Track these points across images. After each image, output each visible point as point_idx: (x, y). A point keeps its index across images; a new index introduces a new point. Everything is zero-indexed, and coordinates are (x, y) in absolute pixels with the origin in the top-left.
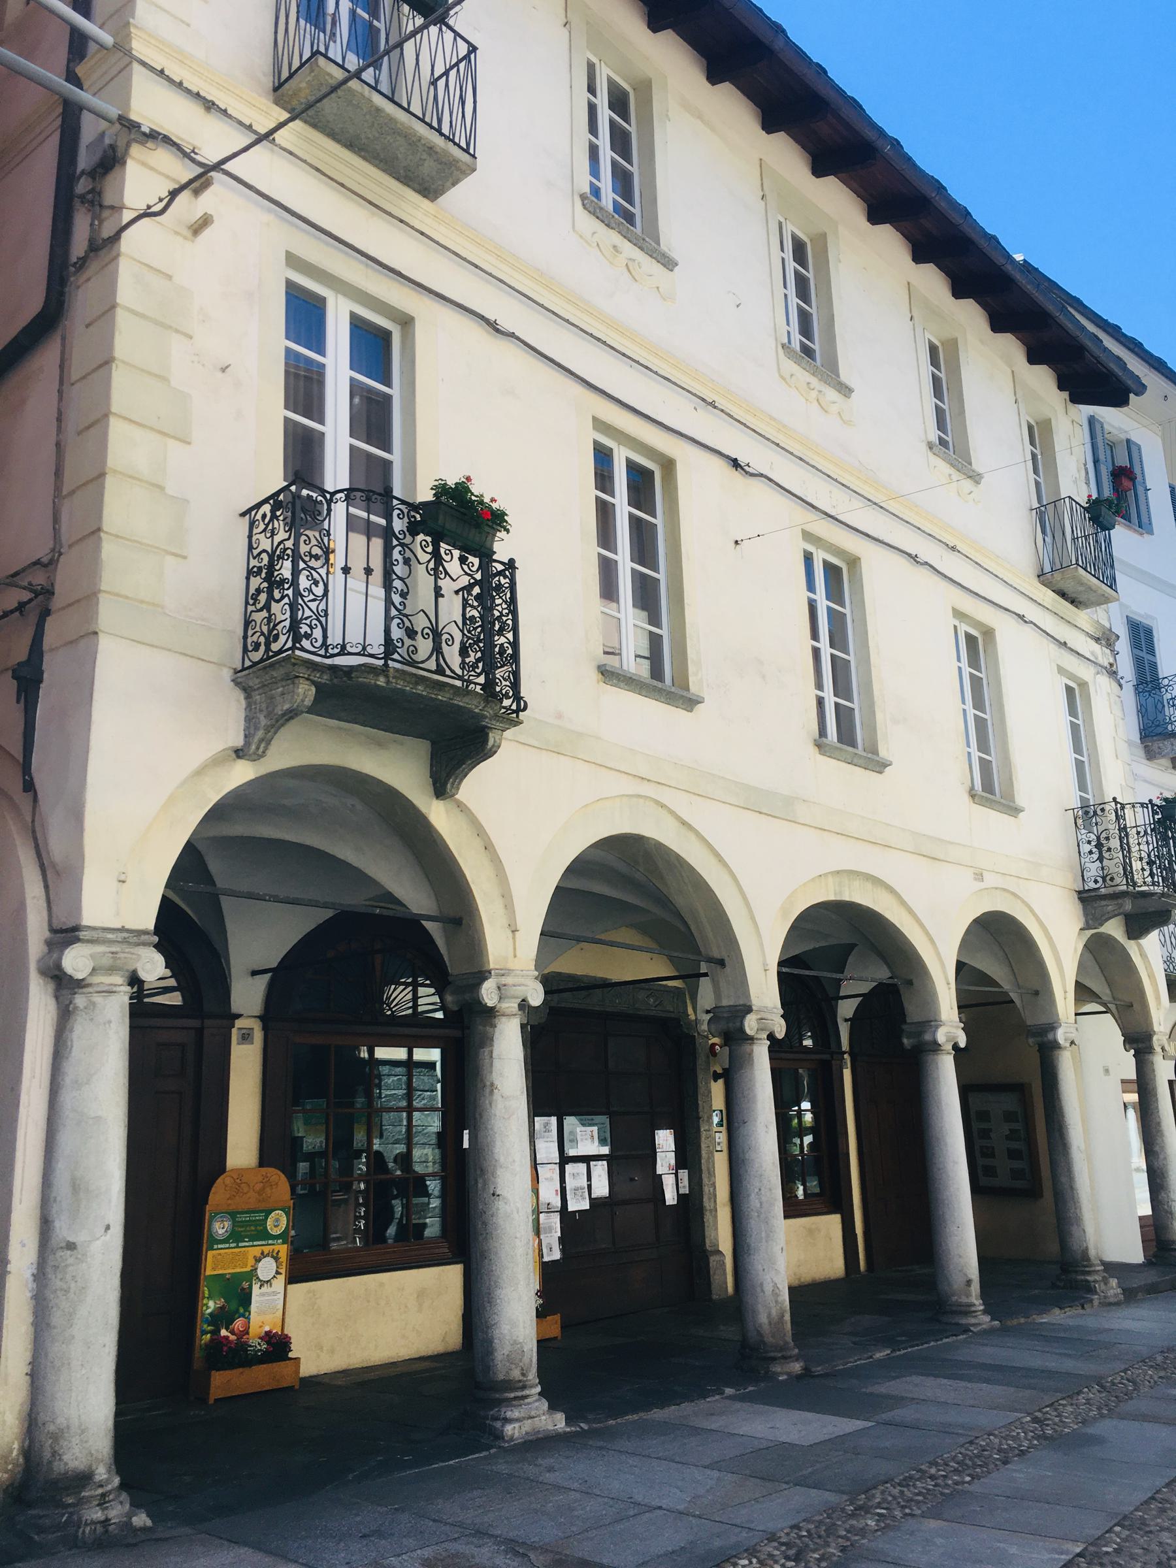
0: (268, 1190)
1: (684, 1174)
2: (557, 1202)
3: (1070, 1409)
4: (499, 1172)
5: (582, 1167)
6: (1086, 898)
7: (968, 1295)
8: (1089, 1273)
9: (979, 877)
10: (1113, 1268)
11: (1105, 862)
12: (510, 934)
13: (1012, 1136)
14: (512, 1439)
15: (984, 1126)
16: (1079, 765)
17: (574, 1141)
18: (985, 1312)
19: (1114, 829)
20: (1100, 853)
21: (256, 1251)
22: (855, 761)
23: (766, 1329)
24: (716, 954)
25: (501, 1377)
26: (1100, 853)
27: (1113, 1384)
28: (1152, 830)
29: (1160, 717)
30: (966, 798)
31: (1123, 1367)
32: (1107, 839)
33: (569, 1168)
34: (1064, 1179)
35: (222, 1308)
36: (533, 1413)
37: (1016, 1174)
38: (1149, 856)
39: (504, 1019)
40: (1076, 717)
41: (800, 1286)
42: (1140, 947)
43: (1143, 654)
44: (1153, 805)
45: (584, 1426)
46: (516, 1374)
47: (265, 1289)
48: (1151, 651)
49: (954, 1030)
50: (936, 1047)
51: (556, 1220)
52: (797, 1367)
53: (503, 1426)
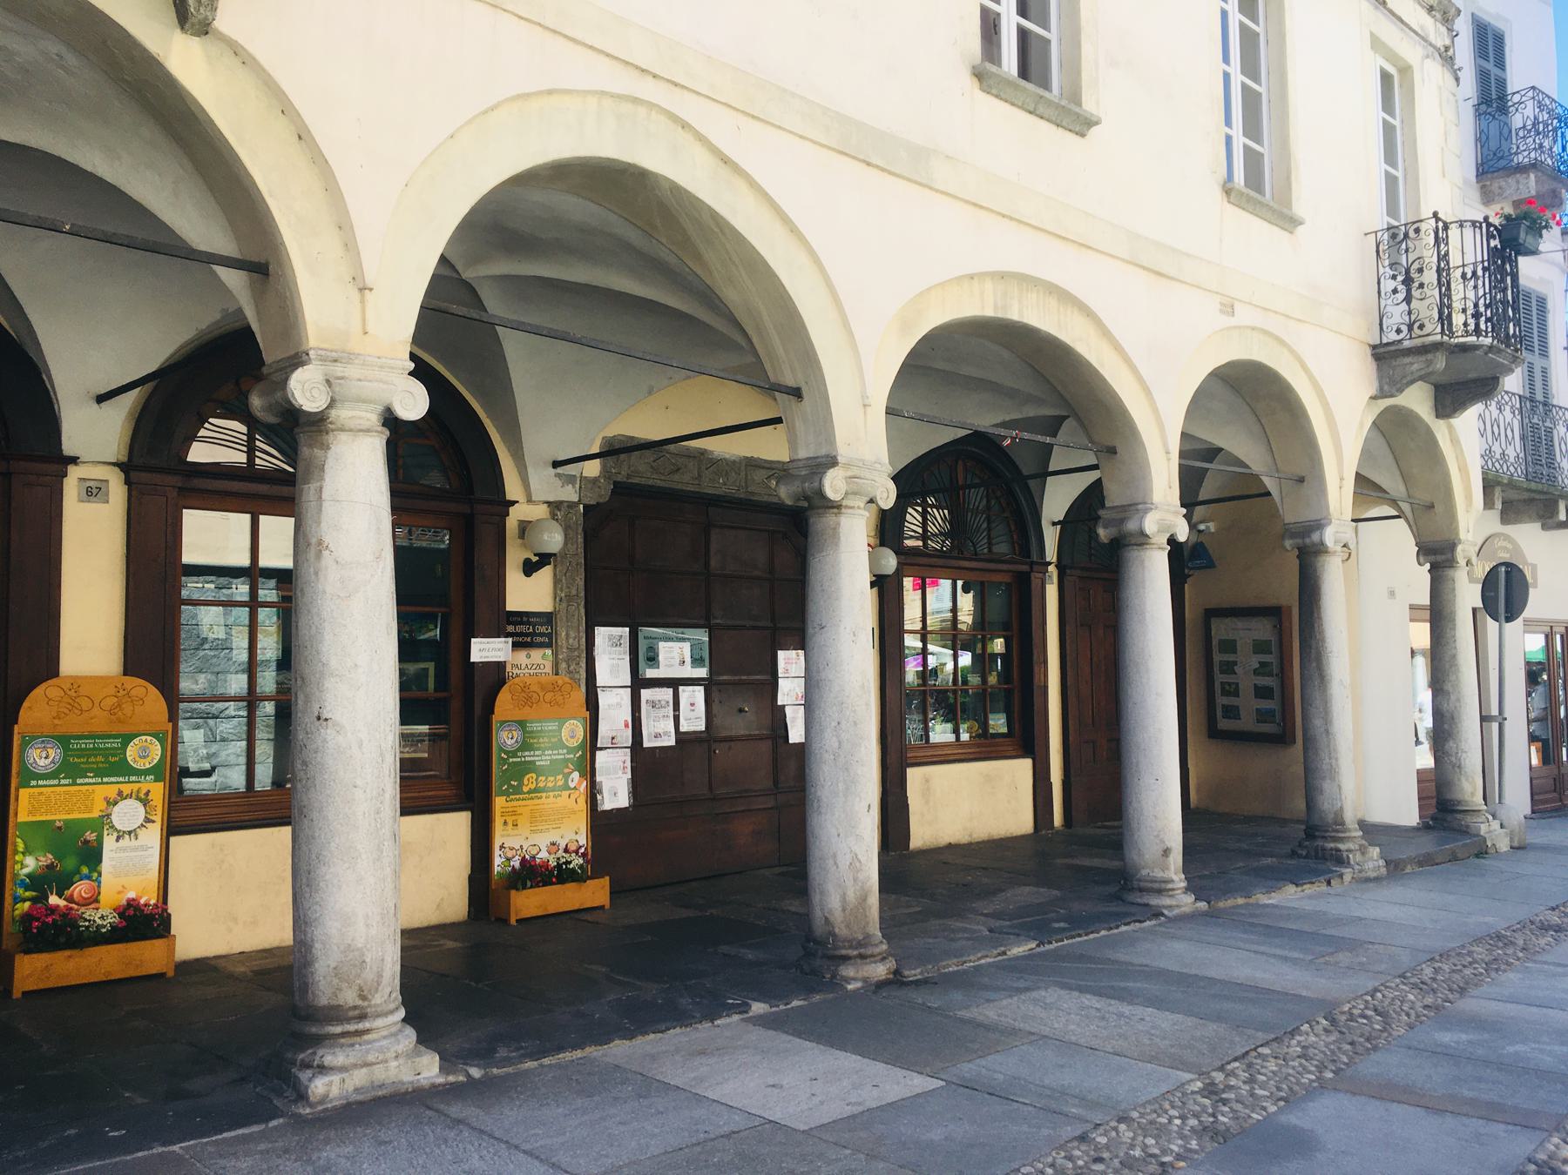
0: (127, 708)
2: (626, 737)
3: (1272, 1065)
5: (667, 694)
6: (1383, 355)
7: (1165, 868)
8: (1341, 840)
9: (1229, 309)
10: (1372, 831)
11: (1414, 304)
12: (356, 295)
13: (1263, 669)
14: (322, 1101)
15: (1230, 658)
16: (1391, 181)
17: (653, 660)
18: (1187, 890)
19: (1431, 258)
20: (1409, 291)
21: (111, 791)
22: (1041, 110)
23: (838, 916)
24: (790, 381)
25: (323, 1001)
26: (1409, 291)
27: (1352, 1018)
28: (1484, 269)
29: (1505, 145)
30: (1218, 194)
31: (1370, 985)
32: (1420, 270)
33: (646, 694)
34: (1318, 722)
35: (51, 867)
36: (371, 1058)
37: (1263, 716)
38: (1476, 305)
39: (343, 437)
40: (1392, 114)
41: (970, 844)
42: (1451, 428)
43: (1490, 66)
44: (1489, 225)
45: (476, 1073)
46: (349, 997)
47: (125, 842)
48: (1500, 63)
49: (1170, 518)
50: (1142, 539)
51: (625, 756)
52: (880, 971)
53: (310, 1080)
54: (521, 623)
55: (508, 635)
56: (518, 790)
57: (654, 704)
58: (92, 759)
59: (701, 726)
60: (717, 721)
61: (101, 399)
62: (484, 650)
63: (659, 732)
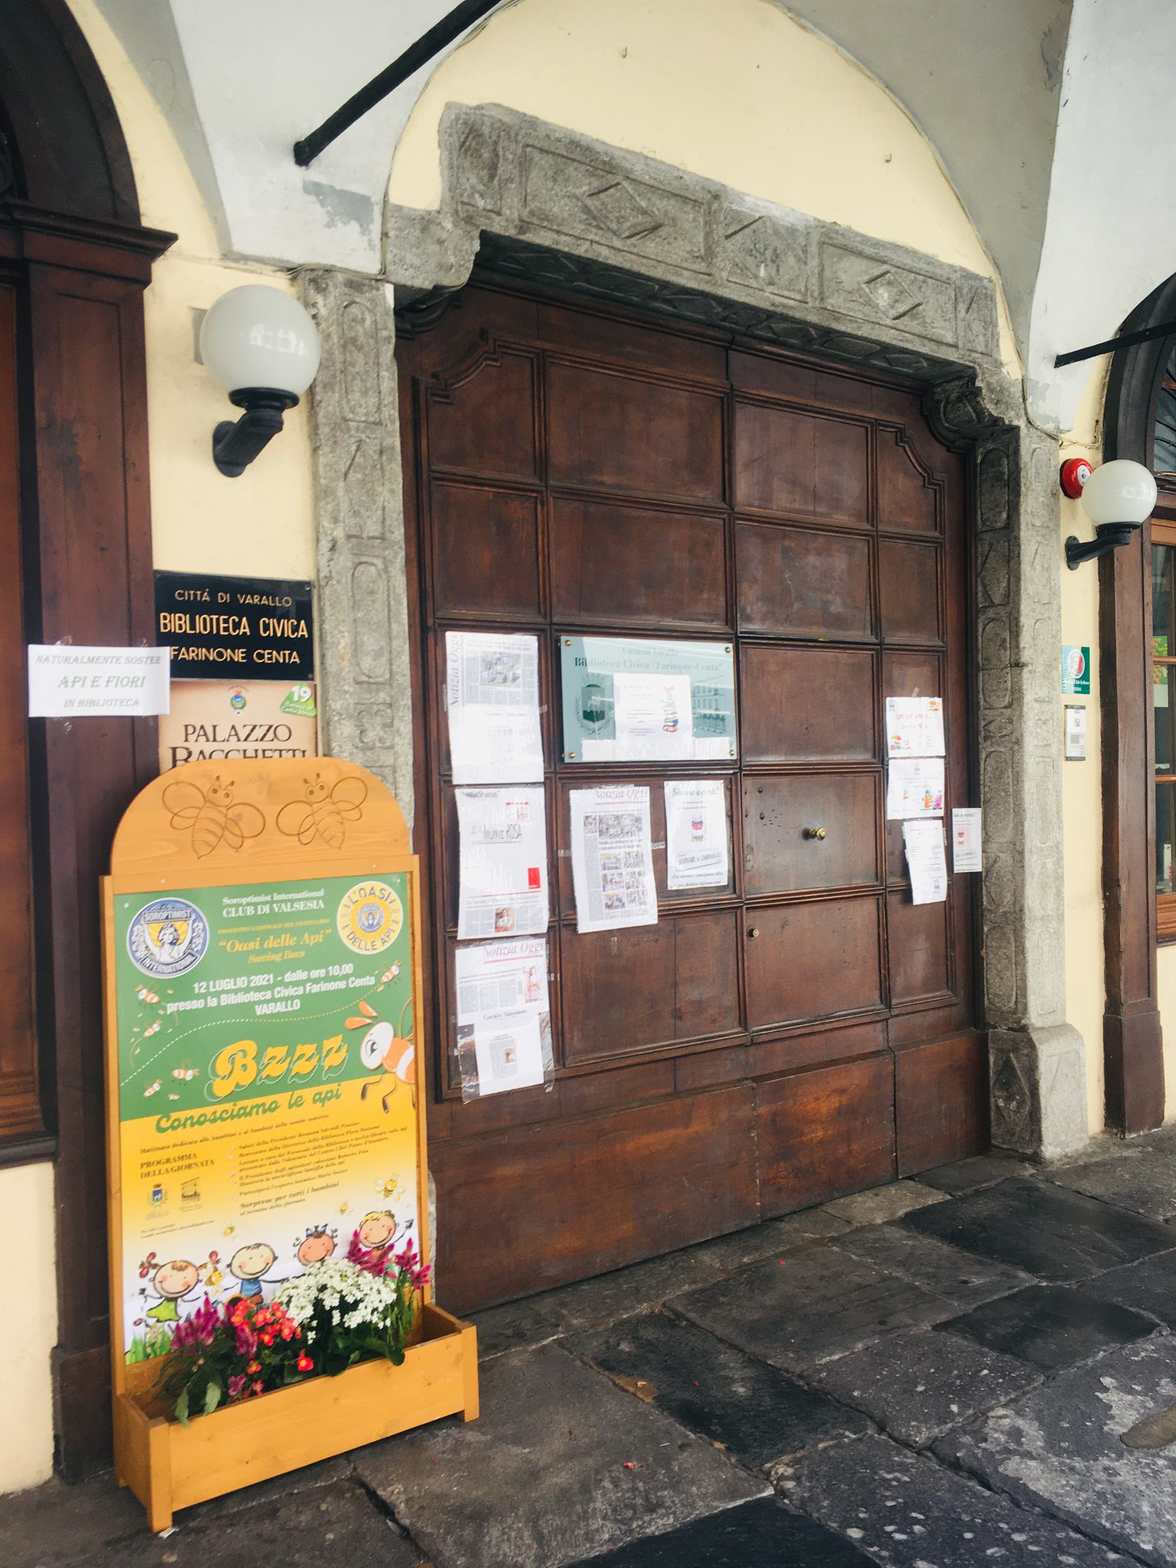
1: (968, 820)
2: (537, 910)
4: (125, 58)
5: (636, 798)
33: (582, 801)
51: (533, 960)
54: (212, 608)
55: (163, 640)
56: (196, 1095)
57: (602, 827)
58: (271, 943)
59: (718, 874)
60: (755, 862)
61: (1062, 360)
62: (77, 680)
63: (618, 902)
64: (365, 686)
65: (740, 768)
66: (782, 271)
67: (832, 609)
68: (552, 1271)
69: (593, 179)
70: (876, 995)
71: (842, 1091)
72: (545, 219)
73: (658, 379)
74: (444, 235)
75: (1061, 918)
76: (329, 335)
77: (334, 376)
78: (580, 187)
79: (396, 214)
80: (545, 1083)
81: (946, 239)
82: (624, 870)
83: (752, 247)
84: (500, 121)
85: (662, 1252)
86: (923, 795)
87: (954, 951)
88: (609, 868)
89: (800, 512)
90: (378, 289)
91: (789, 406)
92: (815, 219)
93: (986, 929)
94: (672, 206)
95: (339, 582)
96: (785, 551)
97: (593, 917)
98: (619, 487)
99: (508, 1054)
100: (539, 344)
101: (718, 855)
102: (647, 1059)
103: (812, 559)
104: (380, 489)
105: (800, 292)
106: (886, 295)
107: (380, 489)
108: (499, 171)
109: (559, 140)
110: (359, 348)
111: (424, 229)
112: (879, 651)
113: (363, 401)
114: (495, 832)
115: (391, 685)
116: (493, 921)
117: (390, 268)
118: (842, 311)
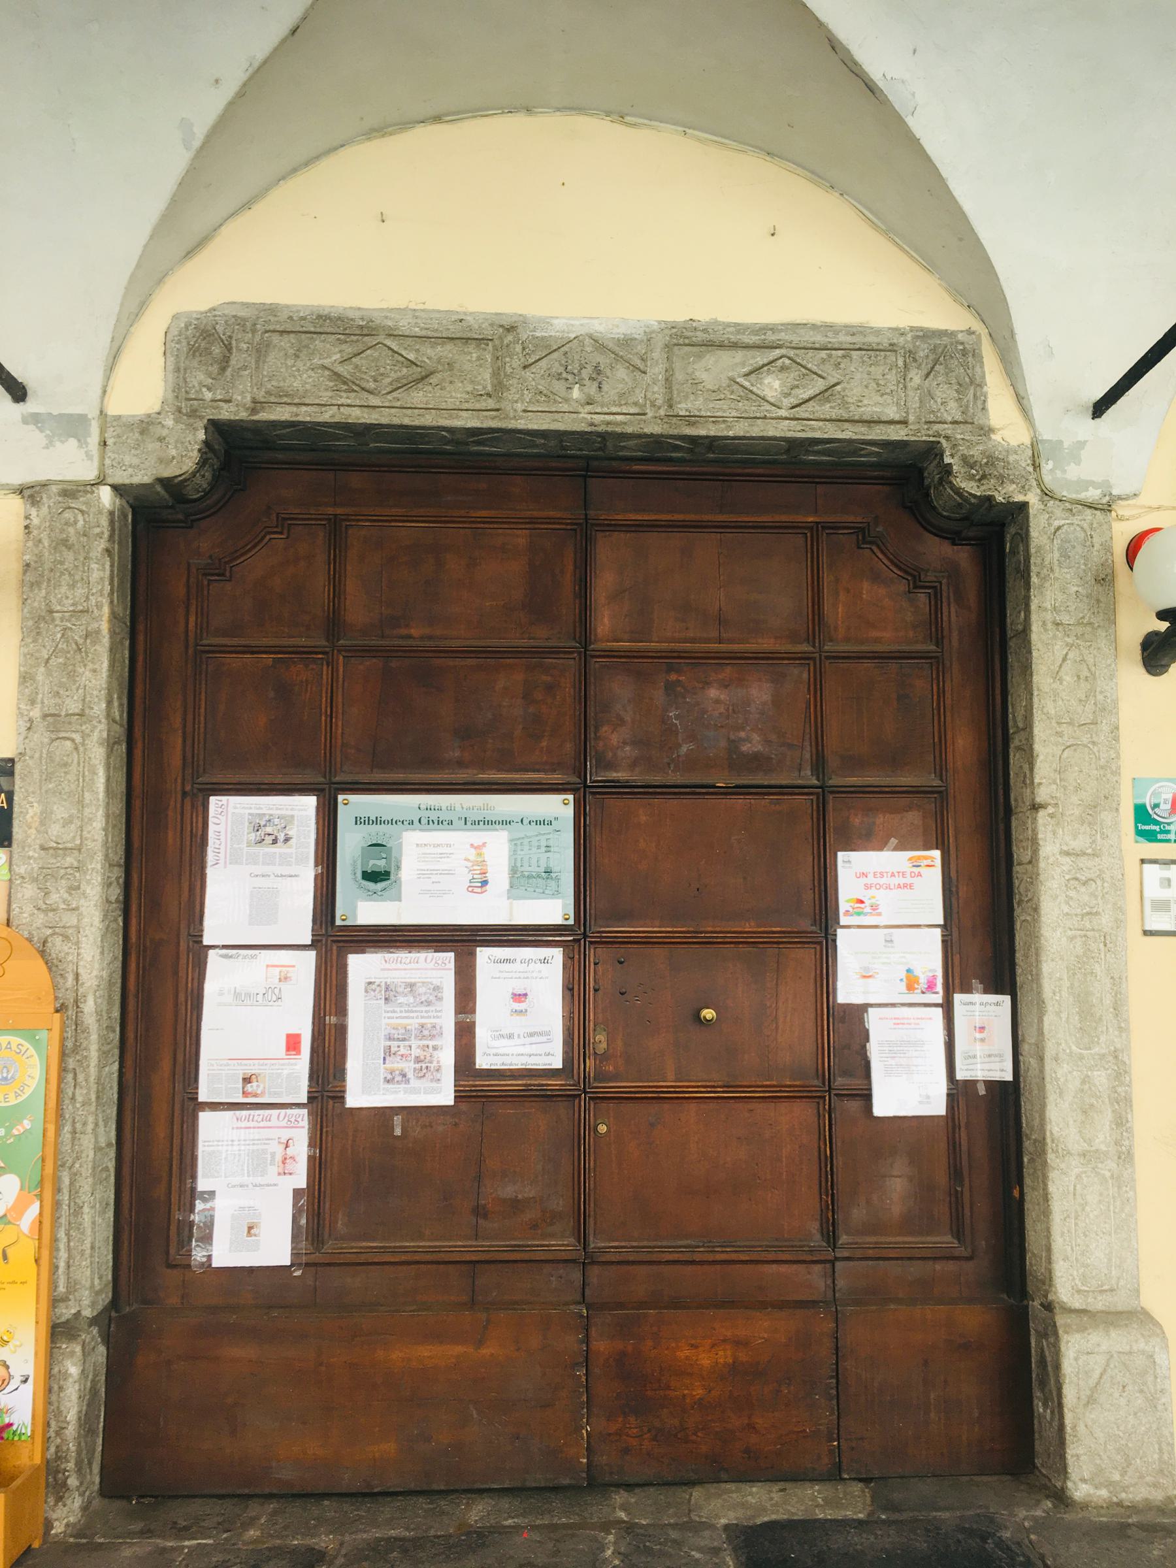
2: (294, 1077)
5: (437, 967)
33: (362, 967)
51: (297, 1132)
61: (1100, 408)
63: (399, 1069)
64: (51, 851)
65: (585, 936)
66: (605, 387)
67: (745, 748)
68: (287, 1474)
69: (344, 347)
70: (814, 1227)
71: (739, 1343)
72: (283, 397)
73: (484, 523)
74: (165, 432)
75: (1126, 1157)
76: (40, 541)
77: (42, 576)
78: (329, 356)
79: (115, 424)
80: (292, 1265)
81: (892, 298)
82: (414, 1043)
83: (561, 369)
84: (234, 316)
85: (435, 1487)
86: (903, 975)
87: (962, 1186)
88: (394, 1040)
89: (693, 640)
90: (93, 492)
91: (671, 526)
92: (659, 322)
93: (1025, 1160)
94: (447, 351)
95: (32, 757)
96: (670, 688)
97: (366, 1090)
98: (430, 638)
99: (250, 1228)
100: (330, 510)
101: (548, 1033)
102: (429, 1257)
103: (713, 693)
104: (81, 670)
105: (636, 404)
106: (777, 384)
107: (81, 670)
108: (233, 362)
109: (303, 319)
110: (69, 548)
111: (142, 433)
112: (822, 795)
113: (69, 594)
114: (248, 995)
115: (80, 850)
116: (240, 1085)
117: (109, 471)
118: (703, 413)
